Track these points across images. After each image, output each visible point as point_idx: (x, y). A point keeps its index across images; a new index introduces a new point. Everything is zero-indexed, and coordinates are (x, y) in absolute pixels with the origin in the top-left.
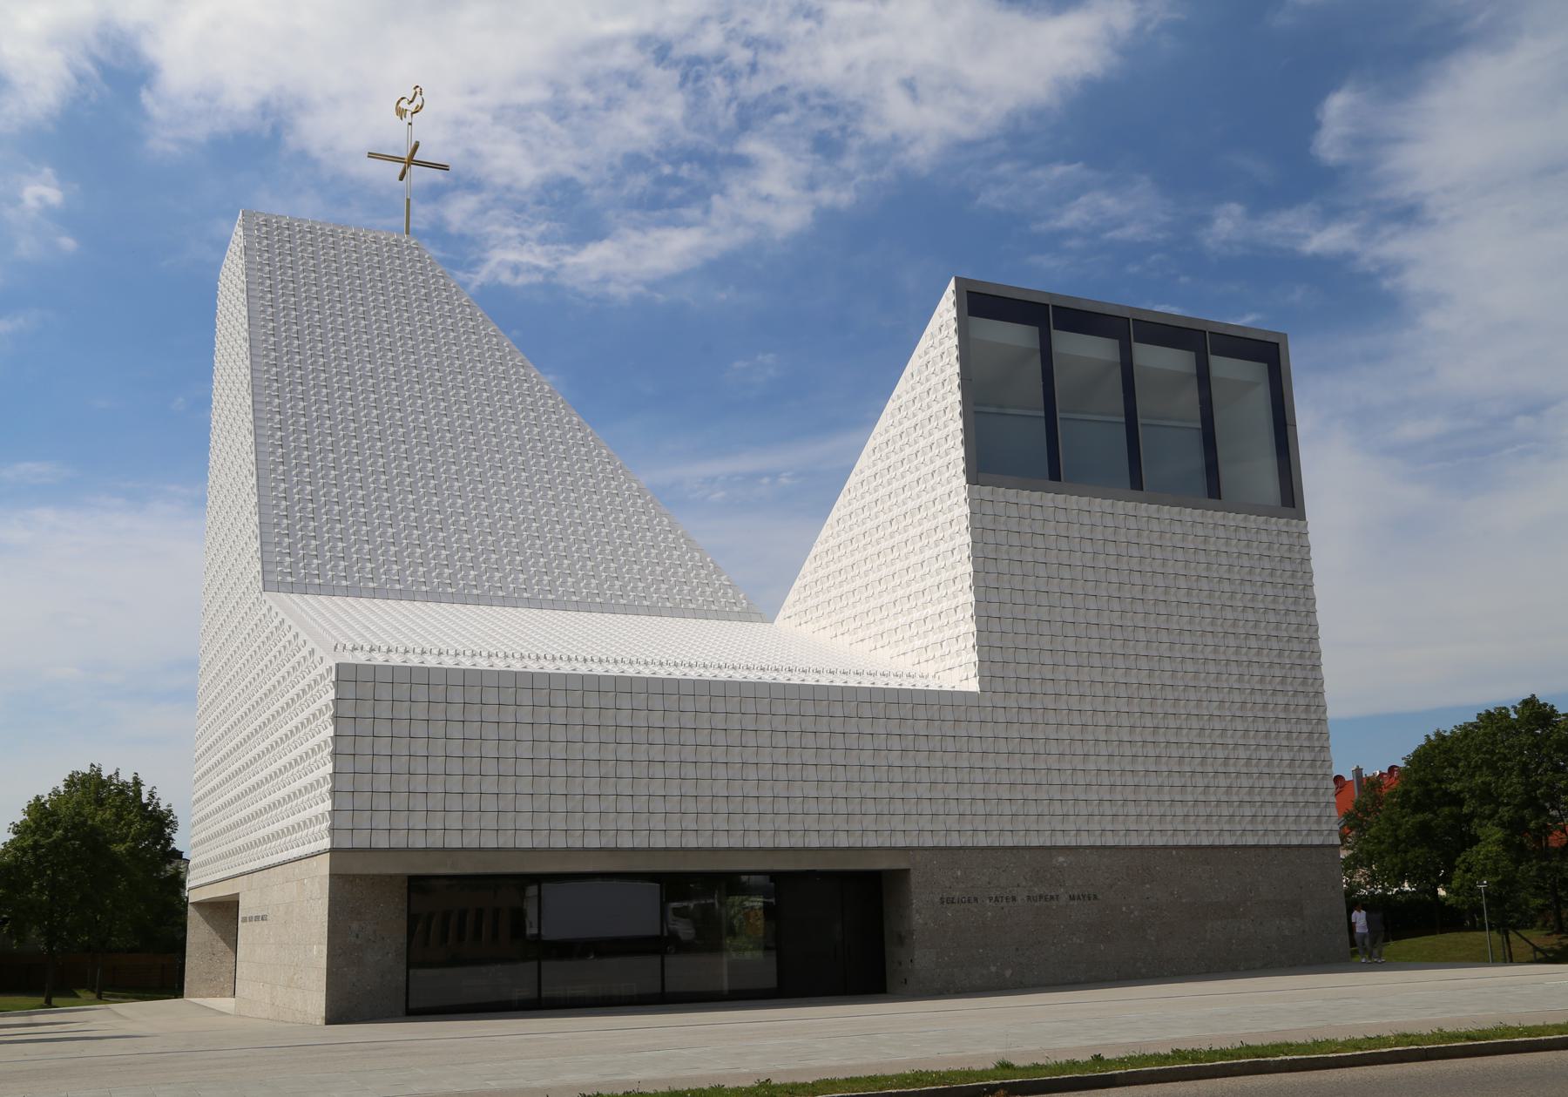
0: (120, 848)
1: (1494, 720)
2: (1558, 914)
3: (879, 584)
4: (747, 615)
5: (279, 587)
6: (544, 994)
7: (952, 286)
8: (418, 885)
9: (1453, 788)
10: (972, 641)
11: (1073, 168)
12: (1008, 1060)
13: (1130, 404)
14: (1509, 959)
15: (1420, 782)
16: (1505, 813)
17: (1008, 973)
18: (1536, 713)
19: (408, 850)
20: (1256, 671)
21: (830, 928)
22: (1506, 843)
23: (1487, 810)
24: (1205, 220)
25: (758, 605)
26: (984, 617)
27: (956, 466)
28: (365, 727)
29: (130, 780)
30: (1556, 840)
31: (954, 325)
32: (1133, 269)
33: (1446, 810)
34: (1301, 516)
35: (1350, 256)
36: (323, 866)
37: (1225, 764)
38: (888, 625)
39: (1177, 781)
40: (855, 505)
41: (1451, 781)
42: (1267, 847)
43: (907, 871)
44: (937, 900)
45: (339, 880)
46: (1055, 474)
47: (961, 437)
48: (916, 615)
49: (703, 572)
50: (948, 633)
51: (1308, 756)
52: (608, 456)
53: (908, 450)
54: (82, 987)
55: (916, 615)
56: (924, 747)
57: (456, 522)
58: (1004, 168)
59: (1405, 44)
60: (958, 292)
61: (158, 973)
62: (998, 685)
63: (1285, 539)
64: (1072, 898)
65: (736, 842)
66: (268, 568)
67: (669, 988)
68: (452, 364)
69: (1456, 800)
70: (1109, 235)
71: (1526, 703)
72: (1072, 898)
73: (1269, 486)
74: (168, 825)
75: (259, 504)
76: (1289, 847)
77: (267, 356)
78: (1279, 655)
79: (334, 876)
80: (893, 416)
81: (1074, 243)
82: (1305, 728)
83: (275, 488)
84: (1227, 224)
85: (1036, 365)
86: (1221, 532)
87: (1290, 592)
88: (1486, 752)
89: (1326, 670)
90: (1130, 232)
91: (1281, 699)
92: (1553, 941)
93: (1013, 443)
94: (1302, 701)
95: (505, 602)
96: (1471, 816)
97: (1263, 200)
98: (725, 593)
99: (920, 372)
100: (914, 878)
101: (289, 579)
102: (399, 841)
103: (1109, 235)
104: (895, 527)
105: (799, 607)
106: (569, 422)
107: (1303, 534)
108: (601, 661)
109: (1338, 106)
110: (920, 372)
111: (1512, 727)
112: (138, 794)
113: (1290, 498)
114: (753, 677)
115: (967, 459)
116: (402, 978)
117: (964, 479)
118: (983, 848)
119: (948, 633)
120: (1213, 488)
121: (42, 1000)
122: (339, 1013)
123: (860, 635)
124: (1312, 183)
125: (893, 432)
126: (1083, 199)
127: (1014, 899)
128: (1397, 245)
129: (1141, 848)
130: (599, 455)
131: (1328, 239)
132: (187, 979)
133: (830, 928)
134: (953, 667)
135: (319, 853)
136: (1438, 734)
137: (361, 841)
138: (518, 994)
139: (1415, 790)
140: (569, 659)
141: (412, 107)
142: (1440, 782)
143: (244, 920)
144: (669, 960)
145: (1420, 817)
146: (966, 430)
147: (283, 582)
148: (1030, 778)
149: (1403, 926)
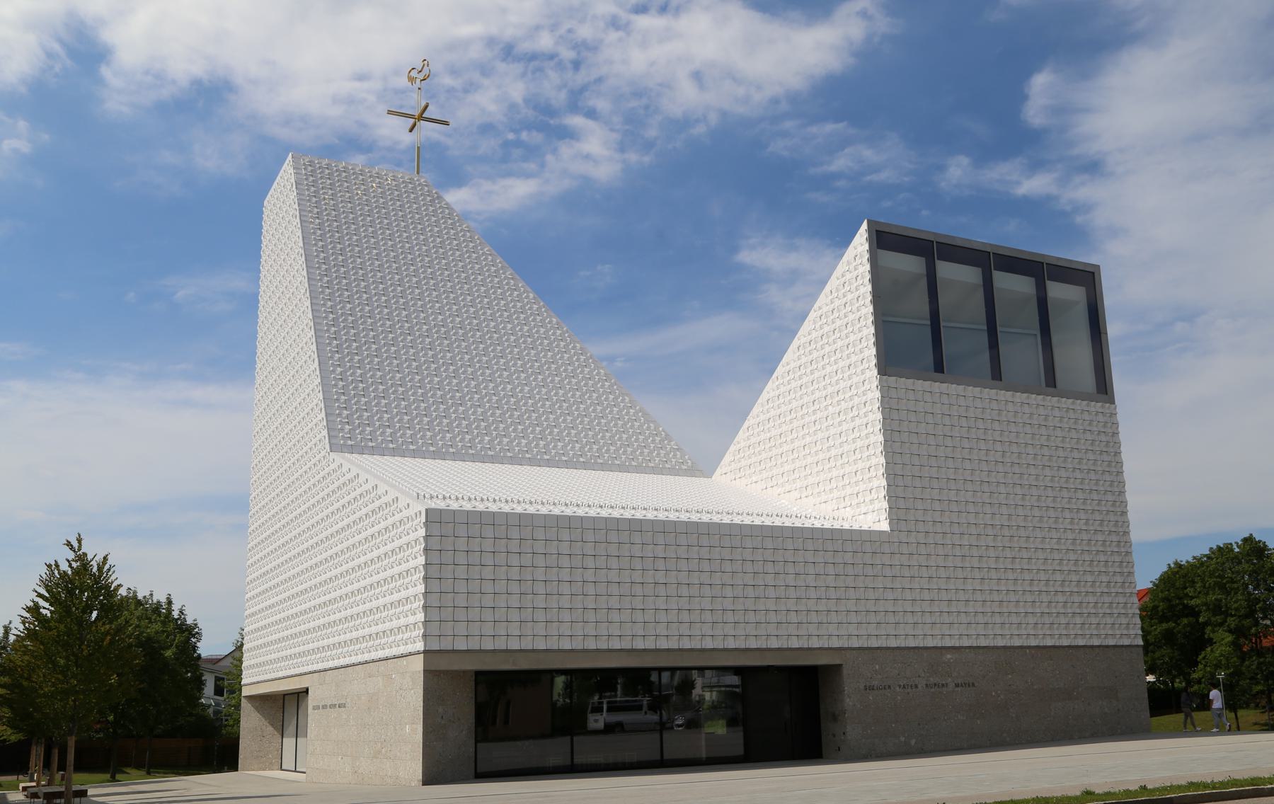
0: (168, 653)
1: (1223, 552)
2: (1269, 697)
3: (803, 446)
4: (693, 471)
6: (576, 761)
7: (865, 226)
8: (479, 674)
9: (1193, 602)
10: (883, 493)
11: (841, 126)
12: (1092, 789)
13: (990, 316)
14: (1238, 729)
15: (1163, 600)
16: (1232, 622)
17: (913, 742)
18: (1254, 548)
19: (481, 651)
20: (1082, 515)
21: (786, 710)
22: (1235, 644)
23: (1219, 619)
24: (942, 168)
25: (700, 467)
26: (892, 475)
27: (869, 361)
28: (448, 557)
29: (163, 600)
30: (1266, 643)
31: (867, 256)
33: (1185, 621)
34: (1112, 401)
35: (1049, 198)
36: (418, 664)
37: (1062, 585)
38: (811, 480)
39: (1029, 598)
40: (782, 389)
41: (1192, 598)
42: (1092, 647)
44: (862, 687)
45: (431, 675)
46: (939, 367)
47: (873, 340)
48: (835, 473)
49: (658, 439)
50: (862, 487)
51: (1119, 579)
52: (581, 349)
53: (827, 349)
54: (128, 765)
55: (835, 473)
56: (591, 565)
57: (375, 390)
58: (789, 125)
59: (1089, 41)
60: (869, 230)
61: (219, 752)
62: (903, 526)
63: (1100, 418)
64: (957, 685)
65: (719, 644)
67: (578, 760)
68: (354, 261)
69: (1194, 613)
70: (868, 178)
71: (1245, 540)
72: (957, 685)
73: (1088, 380)
74: (194, 636)
75: (323, 384)
76: (1107, 647)
77: (319, 268)
78: (1099, 504)
79: (426, 672)
80: (815, 322)
81: (841, 183)
82: (1117, 559)
83: (333, 371)
84: (958, 171)
85: (980, 296)
86: (1056, 412)
87: (1105, 457)
88: (1219, 576)
90: (885, 176)
91: (1100, 537)
92: (1264, 718)
93: (915, 343)
94: (1115, 538)
95: (514, 460)
96: (1206, 624)
97: (985, 154)
98: (675, 455)
99: (837, 290)
100: (845, 672)
101: (350, 442)
102: (474, 644)
103: (868, 178)
104: (781, 400)
105: (733, 466)
106: (550, 322)
107: (1113, 415)
108: (470, 499)
109: (1042, 83)
110: (837, 290)
111: (1236, 557)
112: (169, 611)
113: (1103, 387)
114: (592, 513)
115: (878, 356)
116: (472, 750)
117: (876, 372)
118: (894, 649)
119: (862, 487)
120: (1051, 381)
121: (108, 776)
122: (431, 778)
123: (788, 487)
124: (1020, 141)
125: (814, 334)
127: (916, 686)
128: (1084, 191)
129: (1004, 647)
130: (574, 348)
131: (1035, 185)
132: (241, 757)
133: (786, 710)
134: (870, 514)
135: (418, 653)
136: (1176, 563)
137: (446, 644)
138: (552, 761)
139: (1162, 606)
140: (457, 499)
141: (421, 76)
142: (1180, 599)
143: (315, 708)
144: (575, 738)
145: (1165, 626)
146: (877, 334)
147: (344, 445)
148: (926, 595)
149: (1172, 704)
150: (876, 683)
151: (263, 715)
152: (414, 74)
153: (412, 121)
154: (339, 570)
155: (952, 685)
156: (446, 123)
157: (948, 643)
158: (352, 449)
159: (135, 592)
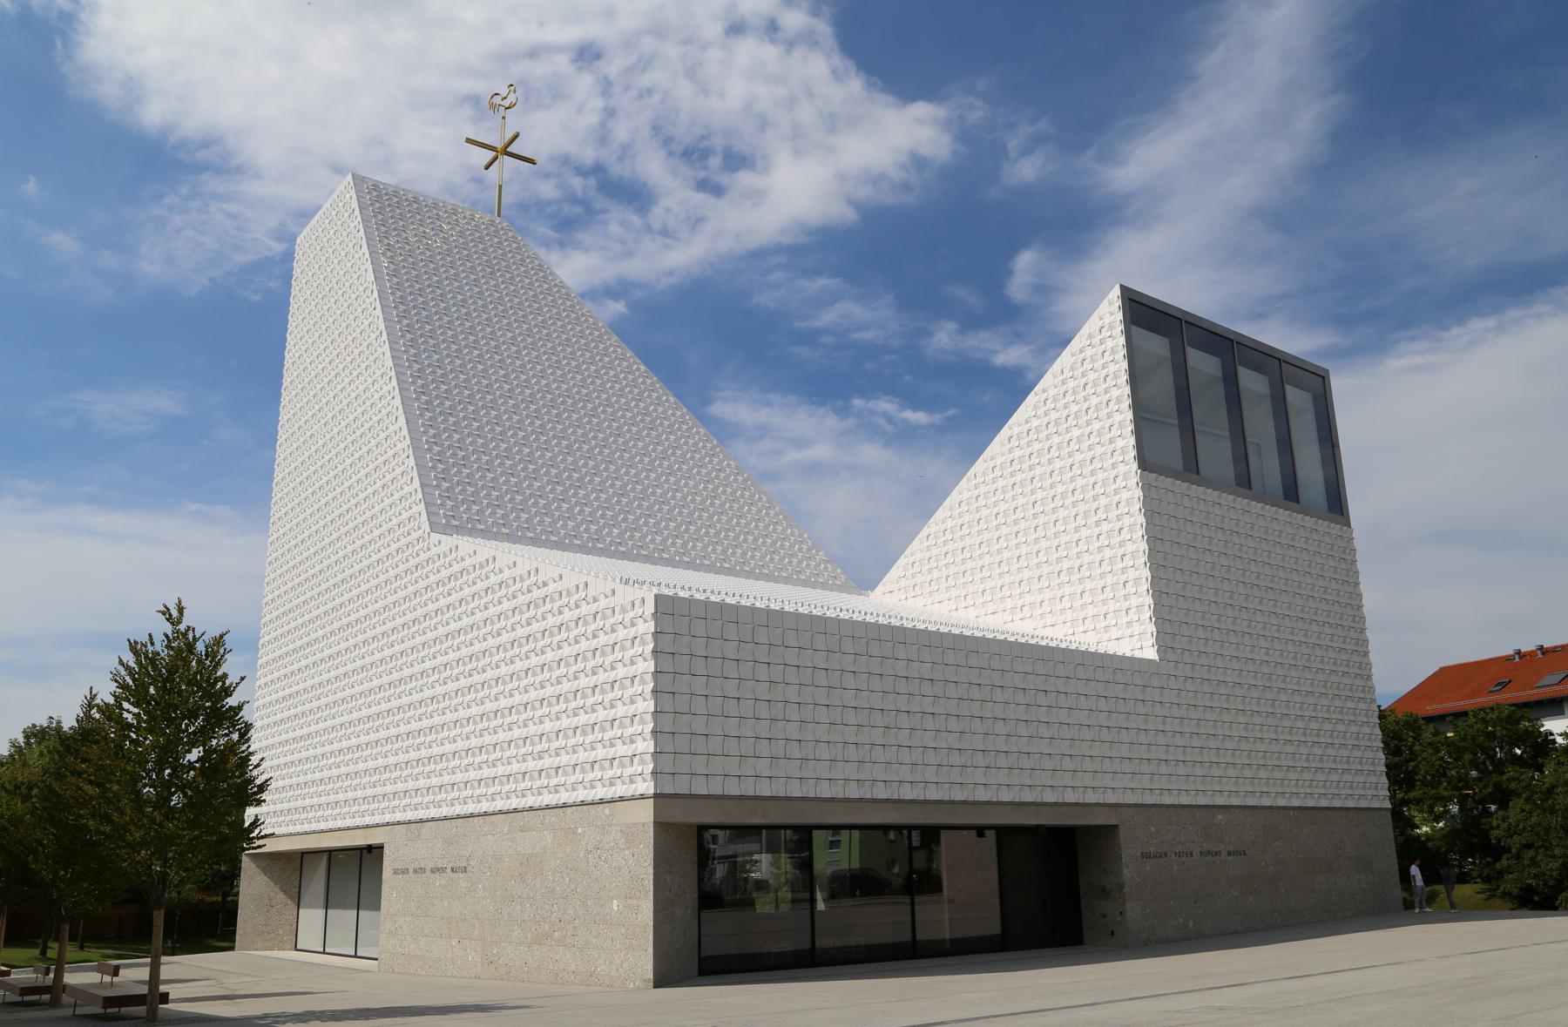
5: (447, 529)
8: (1005, 834)
17: (1191, 924)
25: (865, 583)
32: (869, 366)
36: (645, 814)
43: (1116, 826)
45: (662, 827)
62: (1170, 655)
66: (432, 509)
79: (658, 825)
84: (944, 338)
89: (1373, 657)
90: (869, 335)
97: (970, 322)
109: (1026, 263)
117: (1135, 466)
122: (663, 979)
126: (837, 306)
135: (643, 797)
143: (396, 872)
150: (1152, 850)
151: (271, 878)
152: (497, 100)
153: (491, 154)
154: (308, 706)
155: (1224, 853)
156: (532, 162)
157: (1219, 801)
158: (459, 530)
159: (59, 722)
